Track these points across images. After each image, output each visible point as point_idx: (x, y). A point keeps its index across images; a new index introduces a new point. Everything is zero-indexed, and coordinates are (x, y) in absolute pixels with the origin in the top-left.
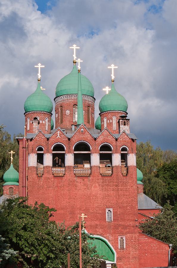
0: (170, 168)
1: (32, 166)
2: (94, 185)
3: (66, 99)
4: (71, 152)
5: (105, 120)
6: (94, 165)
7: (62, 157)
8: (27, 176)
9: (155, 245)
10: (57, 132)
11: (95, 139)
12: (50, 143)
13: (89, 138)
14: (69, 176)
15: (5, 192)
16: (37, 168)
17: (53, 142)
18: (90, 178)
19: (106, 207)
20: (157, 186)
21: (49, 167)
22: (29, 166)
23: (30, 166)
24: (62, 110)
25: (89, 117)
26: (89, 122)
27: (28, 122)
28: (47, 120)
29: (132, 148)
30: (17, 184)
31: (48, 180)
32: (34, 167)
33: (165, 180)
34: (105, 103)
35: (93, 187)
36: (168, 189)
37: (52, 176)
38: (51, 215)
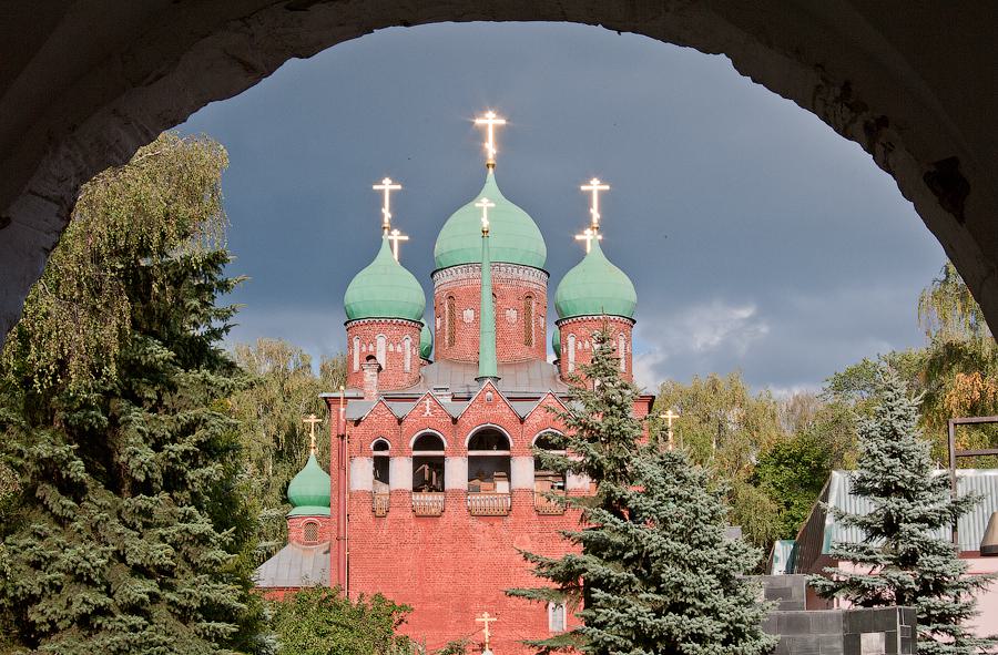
0: (792, 456)
4: (459, 455)
7: (438, 465)
11: (522, 421)
13: (507, 416)
14: (454, 515)
15: (293, 535)
16: (372, 495)
18: (509, 520)
20: (753, 513)
21: (404, 492)
24: (451, 307)
25: (530, 327)
26: (528, 343)
28: (407, 343)
30: (326, 511)
32: (364, 492)
33: (777, 493)
36: (786, 522)
37: (411, 514)
38: (401, 621)
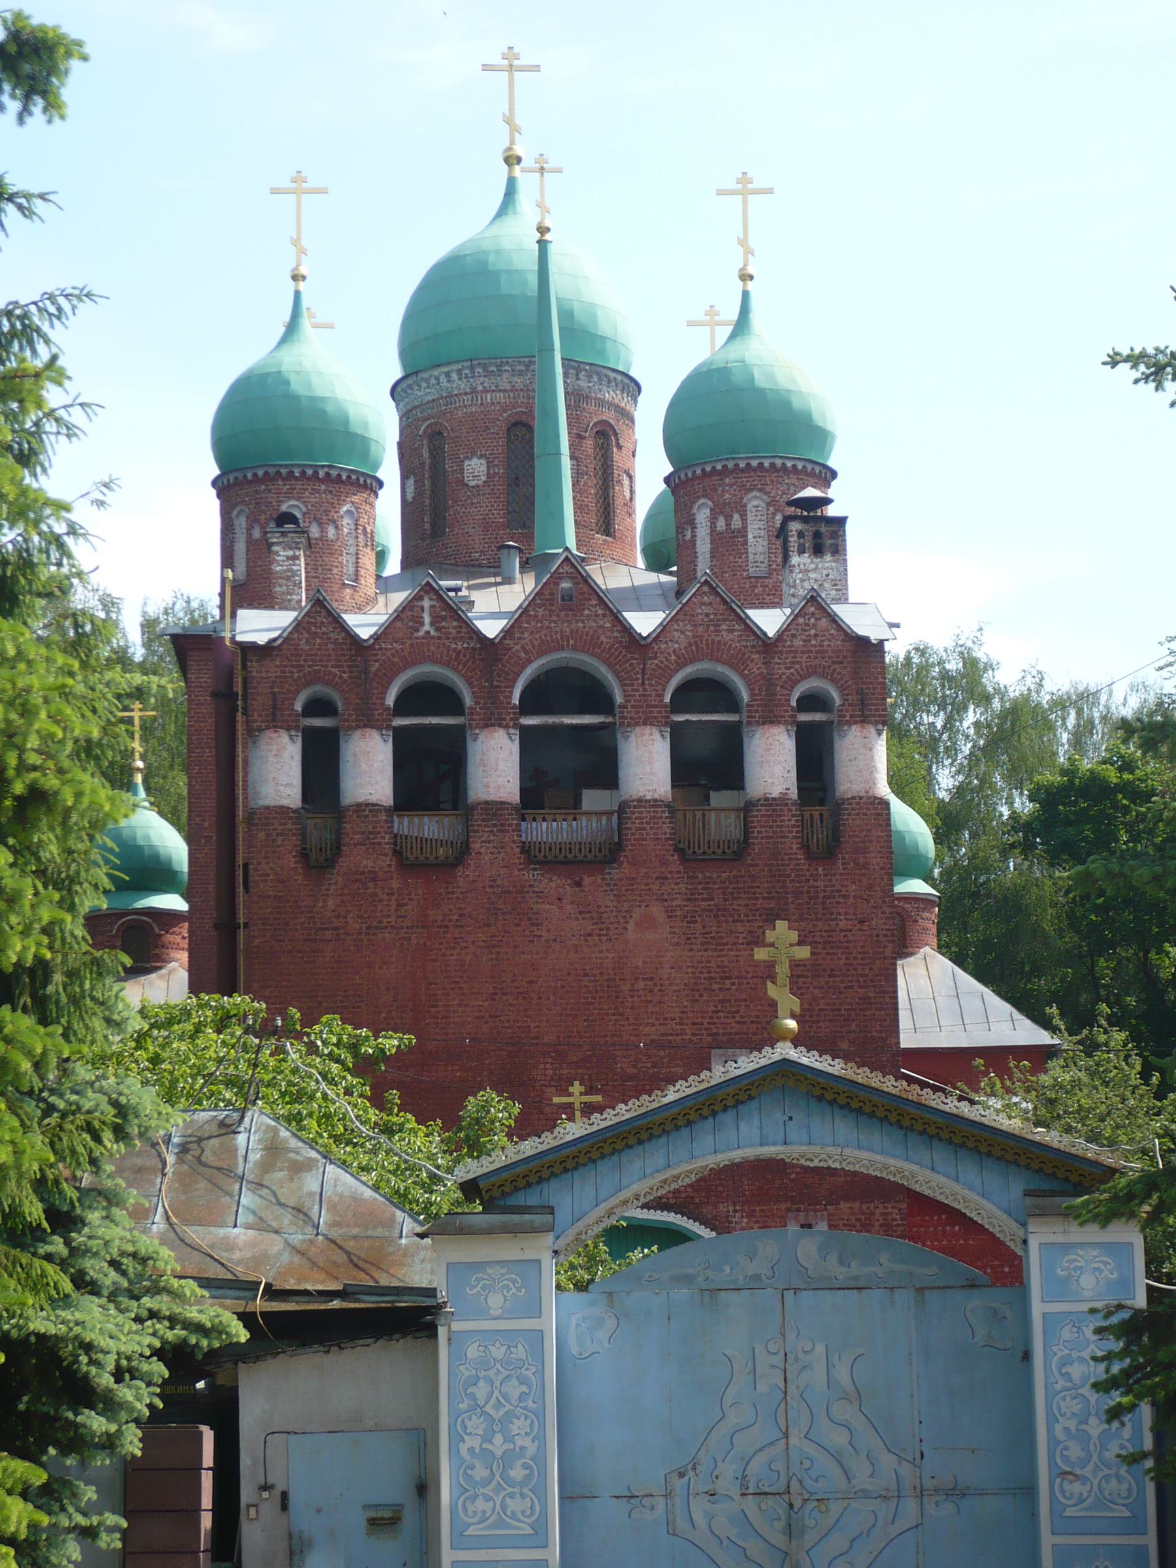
1: (272, 803)
2: (637, 913)
3: (464, 385)
4: (500, 723)
5: (702, 516)
6: (641, 794)
8: (246, 866)
9: (1006, 1269)
10: (419, 603)
12: (378, 670)
14: (490, 857)
17: (396, 659)
19: (709, 1039)
22: (251, 804)
23: (262, 803)
27: (237, 530)
29: (861, 693)
31: (371, 884)
34: (561, 295)
35: (637, 924)
37: (387, 862)
